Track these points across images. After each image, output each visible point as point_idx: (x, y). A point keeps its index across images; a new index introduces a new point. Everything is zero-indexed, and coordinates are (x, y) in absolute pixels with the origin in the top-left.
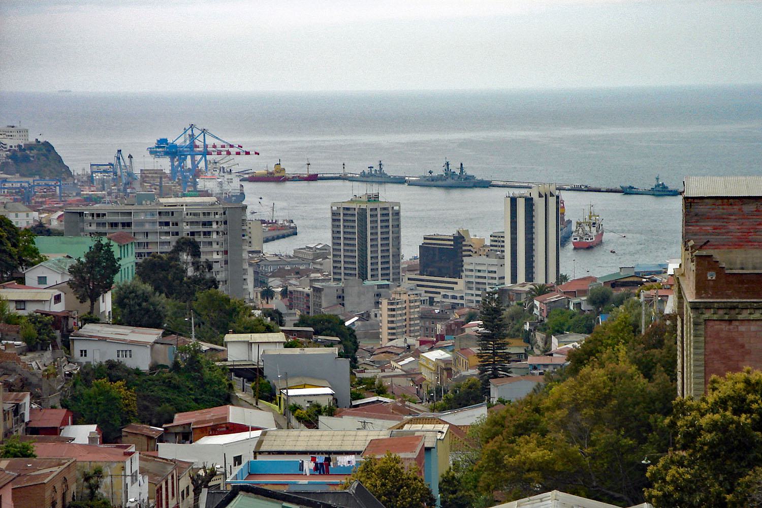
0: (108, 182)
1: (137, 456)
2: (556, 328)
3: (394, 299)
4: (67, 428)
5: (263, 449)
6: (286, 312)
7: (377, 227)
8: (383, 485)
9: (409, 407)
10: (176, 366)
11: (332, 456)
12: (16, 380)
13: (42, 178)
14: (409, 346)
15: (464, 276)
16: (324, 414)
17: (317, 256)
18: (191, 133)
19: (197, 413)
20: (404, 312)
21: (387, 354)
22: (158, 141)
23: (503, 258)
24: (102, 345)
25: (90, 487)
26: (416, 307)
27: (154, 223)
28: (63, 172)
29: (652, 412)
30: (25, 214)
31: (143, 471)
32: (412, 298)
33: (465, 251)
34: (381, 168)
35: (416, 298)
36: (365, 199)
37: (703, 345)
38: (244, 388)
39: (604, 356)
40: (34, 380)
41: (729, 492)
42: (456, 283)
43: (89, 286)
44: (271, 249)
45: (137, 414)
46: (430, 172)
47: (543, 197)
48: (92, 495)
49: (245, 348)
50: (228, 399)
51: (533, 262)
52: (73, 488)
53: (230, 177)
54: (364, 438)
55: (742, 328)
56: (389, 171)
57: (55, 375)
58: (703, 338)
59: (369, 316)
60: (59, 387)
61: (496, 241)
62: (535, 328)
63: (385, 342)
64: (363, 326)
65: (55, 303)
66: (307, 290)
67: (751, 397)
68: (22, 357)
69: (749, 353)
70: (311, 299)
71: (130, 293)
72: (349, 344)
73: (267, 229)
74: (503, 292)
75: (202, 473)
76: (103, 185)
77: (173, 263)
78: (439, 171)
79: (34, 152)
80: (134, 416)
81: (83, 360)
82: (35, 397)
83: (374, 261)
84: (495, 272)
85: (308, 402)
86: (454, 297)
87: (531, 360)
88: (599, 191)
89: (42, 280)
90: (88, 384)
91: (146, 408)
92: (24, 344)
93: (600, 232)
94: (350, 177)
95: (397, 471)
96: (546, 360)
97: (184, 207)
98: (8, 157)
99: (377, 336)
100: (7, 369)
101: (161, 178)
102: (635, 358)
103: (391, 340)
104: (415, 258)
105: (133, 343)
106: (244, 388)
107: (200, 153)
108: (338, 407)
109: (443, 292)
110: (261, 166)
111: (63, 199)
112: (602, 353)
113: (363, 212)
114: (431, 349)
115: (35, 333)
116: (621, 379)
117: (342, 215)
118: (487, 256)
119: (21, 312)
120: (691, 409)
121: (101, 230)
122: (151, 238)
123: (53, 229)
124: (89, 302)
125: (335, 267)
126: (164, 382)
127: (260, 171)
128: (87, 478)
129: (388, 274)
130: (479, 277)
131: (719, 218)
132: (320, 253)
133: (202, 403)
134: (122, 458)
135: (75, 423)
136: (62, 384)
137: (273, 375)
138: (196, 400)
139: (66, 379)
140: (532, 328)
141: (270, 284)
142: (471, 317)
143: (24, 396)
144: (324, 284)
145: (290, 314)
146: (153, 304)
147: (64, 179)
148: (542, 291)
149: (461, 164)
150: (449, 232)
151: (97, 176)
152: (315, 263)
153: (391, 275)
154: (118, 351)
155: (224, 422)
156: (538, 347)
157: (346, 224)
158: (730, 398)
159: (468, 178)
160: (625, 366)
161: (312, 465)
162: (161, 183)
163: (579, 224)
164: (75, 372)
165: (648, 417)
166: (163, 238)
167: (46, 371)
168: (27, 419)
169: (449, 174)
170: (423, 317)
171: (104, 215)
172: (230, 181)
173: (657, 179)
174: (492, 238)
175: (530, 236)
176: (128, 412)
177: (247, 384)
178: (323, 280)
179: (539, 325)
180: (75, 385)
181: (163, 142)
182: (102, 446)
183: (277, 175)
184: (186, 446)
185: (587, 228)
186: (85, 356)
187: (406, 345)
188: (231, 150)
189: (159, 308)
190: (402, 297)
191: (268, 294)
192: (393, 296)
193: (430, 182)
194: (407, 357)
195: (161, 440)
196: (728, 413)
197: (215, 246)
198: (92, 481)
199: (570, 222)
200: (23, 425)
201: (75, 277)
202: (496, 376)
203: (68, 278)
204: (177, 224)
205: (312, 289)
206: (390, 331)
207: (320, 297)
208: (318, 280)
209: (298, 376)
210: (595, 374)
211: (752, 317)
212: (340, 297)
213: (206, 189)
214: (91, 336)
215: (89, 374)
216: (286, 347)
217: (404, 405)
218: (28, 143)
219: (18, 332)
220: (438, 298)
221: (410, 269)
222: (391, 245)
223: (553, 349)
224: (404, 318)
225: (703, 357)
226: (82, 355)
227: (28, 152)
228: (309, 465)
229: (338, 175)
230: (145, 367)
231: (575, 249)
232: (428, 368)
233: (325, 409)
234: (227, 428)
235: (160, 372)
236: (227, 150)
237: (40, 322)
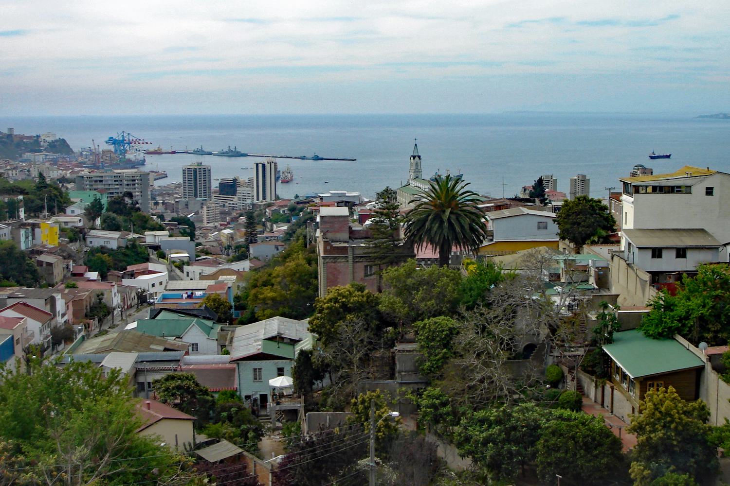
5: (167, 289)
8: (214, 305)
10: (127, 247)
11: (194, 292)
13: (62, 154)
19: (136, 266)
23: (253, 188)
25: (99, 299)
27: (111, 180)
29: (311, 278)
31: (118, 292)
40: (73, 254)
41: (333, 328)
44: (157, 184)
48: (100, 302)
49: (153, 237)
50: (147, 260)
52: (93, 300)
57: (81, 252)
63: (205, 224)
66: (173, 202)
67: (339, 298)
69: (341, 272)
74: (253, 205)
75: (140, 290)
78: (226, 150)
79: (58, 143)
81: (91, 245)
82: (74, 261)
86: (233, 204)
87: (266, 235)
89: (73, 212)
90: (93, 255)
91: (116, 264)
95: (219, 299)
96: (271, 235)
98: (48, 145)
99: (202, 221)
104: (217, 187)
109: (229, 202)
113: (195, 170)
114: (225, 229)
119: (66, 227)
120: (321, 301)
121: (92, 184)
127: (152, 150)
128: (98, 296)
131: (331, 223)
132: (178, 186)
133: (137, 262)
134: (110, 287)
135: (89, 271)
138: (135, 260)
142: (241, 215)
143: (70, 262)
148: (269, 205)
150: (230, 177)
151: (84, 153)
158: (333, 298)
159: (238, 152)
160: (302, 262)
161: (186, 296)
163: (283, 172)
169: (231, 151)
172: (139, 155)
179: (268, 220)
191: (156, 204)
193: (222, 154)
196: (332, 304)
197: (137, 189)
198: (100, 297)
202: (252, 243)
209: (175, 249)
210: (291, 264)
215: (94, 251)
216: (169, 237)
220: (227, 205)
228: (185, 296)
230: (115, 247)
236: (137, 141)
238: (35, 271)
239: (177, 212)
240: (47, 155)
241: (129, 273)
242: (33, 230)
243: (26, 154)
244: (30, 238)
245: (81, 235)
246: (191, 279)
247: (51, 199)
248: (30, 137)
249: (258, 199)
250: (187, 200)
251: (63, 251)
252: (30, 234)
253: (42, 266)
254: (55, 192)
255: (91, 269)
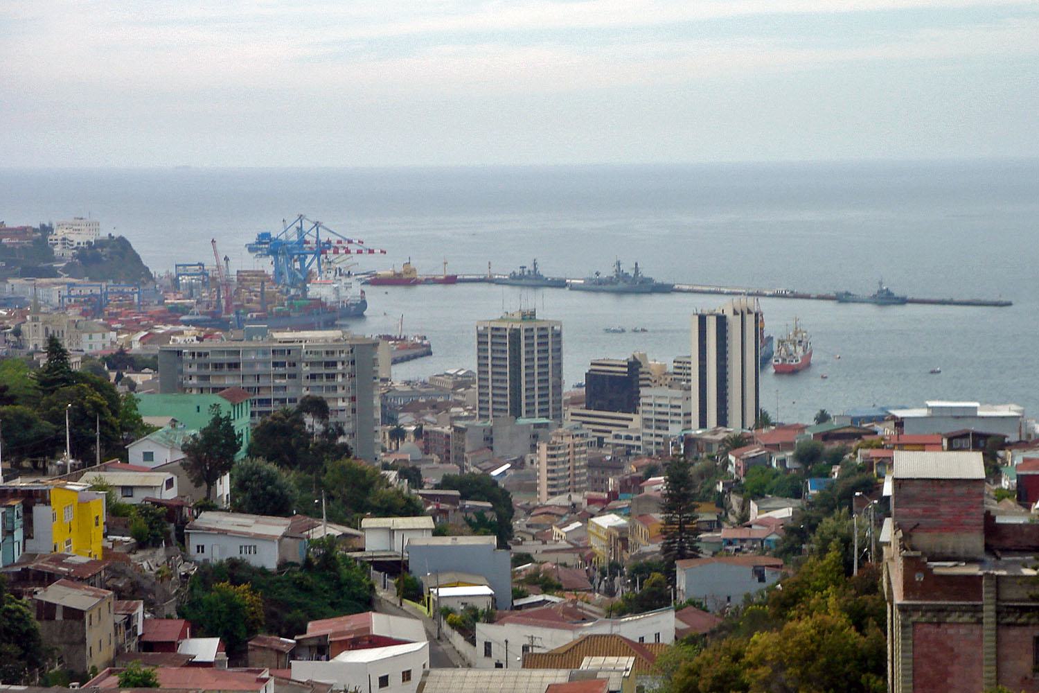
0: (197, 286)
1: (271, 682)
2: (756, 490)
3: (554, 443)
4: (185, 641)
6: (421, 458)
7: (533, 352)
9: (582, 608)
10: (308, 564)
12: (125, 584)
14: (574, 505)
15: (640, 412)
16: (482, 619)
17: (458, 385)
18: (300, 226)
20: (567, 458)
21: (548, 516)
22: (259, 236)
23: (689, 389)
24: (223, 540)
26: (581, 453)
27: (265, 363)
28: (143, 275)
29: (865, 671)
30: (100, 335)
32: (577, 440)
33: (642, 379)
34: (535, 269)
35: (582, 442)
36: (518, 316)
37: (911, 647)
38: (385, 585)
39: (812, 601)
40: (147, 584)
42: (631, 420)
43: (206, 468)
44: (400, 375)
45: (264, 623)
46: (597, 274)
47: (738, 314)
50: (368, 603)
51: (726, 394)
53: (348, 280)
54: (539, 680)
55: (951, 631)
56: (547, 271)
57: (170, 577)
58: (910, 642)
59: (523, 463)
60: (175, 591)
61: (680, 368)
62: (729, 488)
63: (543, 498)
64: (515, 475)
65: (167, 488)
66: (447, 430)
68: (132, 556)
69: (957, 656)
70: (452, 442)
71: (254, 474)
72: (504, 510)
73: (395, 348)
76: (192, 291)
77: (296, 426)
78: (607, 272)
79: (106, 250)
80: (261, 625)
81: (200, 557)
82: (149, 605)
83: (529, 393)
84: (679, 407)
85: (462, 604)
86: (629, 438)
87: (726, 533)
88: (808, 297)
89: (148, 456)
92: (133, 541)
93: (808, 352)
94: (496, 279)
97: (304, 344)
99: (533, 489)
100: (115, 571)
101: (263, 283)
102: (846, 605)
103: (552, 494)
104: (579, 386)
105: (259, 537)
106: (385, 585)
107: (311, 251)
108: (497, 609)
109: (615, 431)
110: (385, 269)
111: (142, 310)
112: (809, 597)
113: (515, 335)
114: (602, 512)
115: (145, 527)
116: (830, 633)
117: (489, 336)
118: (670, 386)
119: (128, 501)
122: (263, 382)
123: (135, 355)
124: (205, 486)
125: (480, 402)
126: (294, 583)
127: (385, 272)
129: (547, 410)
130: (660, 413)
132: (462, 382)
135: (193, 635)
136: (177, 587)
137: (420, 572)
138: (332, 605)
139: (182, 582)
140: (726, 490)
141: (400, 422)
142: (652, 471)
144: (467, 422)
145: (426, 461)
146: (279, 487)
147: (144, 283)
148: (738, 443)
149: (636, 264)
151: (184, 280)
152: (455, 394)
153: (551, 411)
154: (241, 547)
155: (367, 634)
156: (734, 513)
157: (494, 347)
160: (837, 619)
162: (263, 289)
163: (781, 342)
164: (192, 573)
165: (860, 677)
166: (277, 381)
167: (158, 572)
168: (140, 632)
170: (591, 465)
171: (206, 354)
172: (348, 286)
173: (881, 283)
174: (676, 364)
175: (722, 363)
176: (253, 622)
177: (389, 580)
178: (467, 418)
179: (734, 487)
180: (192, 589)
181: (264, 237)
182: (231, 670)
183: (405, 277)
184: (322, 664)
185: (792, 348)
186: (203, 552)
187: (570, 504)
188: (350, 247)
189: (287, 492)
190: (564, 441)
191: (398, 434)
192: (554, 439)
193: (596, 286)
194: (572, 521)
195: (293, 656)
197: (340, 391)
199: (770, 339)
200: (136, 639)
201: (189, 455)
203: (181, 456)
204: (294, 365)
205: (453, 429)
206: (550, 482)
207: (463, 440)
208: (459, 418)
210: (803, 627)
211: (961, 620)
212: (487, 439)
213: (318, 297)
214: (210, 529)
215: (209, 575)
217: (575, 607)
218: (98, 238)
219: (126, 527)
220: (609, 439)
221: (574, 402)
222: (550, 374)
223: (752, 519)
224: (567, 466)
225: (911, 661)
226: (198, 551)
227: (100, 250)
229: (482, 277)
230: (272, 565)
231: (776, 373)
232: (597, 536)
233: (483, 612)
234: (370, 641)
235: (289, 571)
236: (343, 246)
237: (152, 514)
238: (31, 634)
239: (460, 460)
240: (72, 285)
241: (312, 643)
242: (28, 510)
243: (11, 281)
244: (19, 535)
245: (172, 526)
246: (499, 665)
247: (83, 418)
248: (23, 231)
249: (703, 424)
250: (490, 423)
251: (117, 574)
252: (18, 523)
253: (51, 617)
254: (97, 397)
255: (199, 630)
